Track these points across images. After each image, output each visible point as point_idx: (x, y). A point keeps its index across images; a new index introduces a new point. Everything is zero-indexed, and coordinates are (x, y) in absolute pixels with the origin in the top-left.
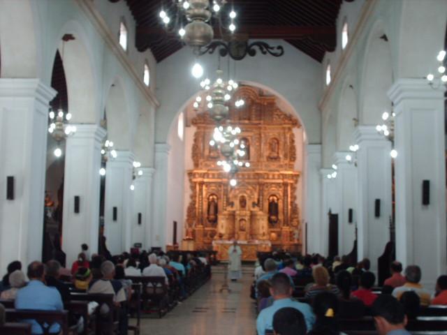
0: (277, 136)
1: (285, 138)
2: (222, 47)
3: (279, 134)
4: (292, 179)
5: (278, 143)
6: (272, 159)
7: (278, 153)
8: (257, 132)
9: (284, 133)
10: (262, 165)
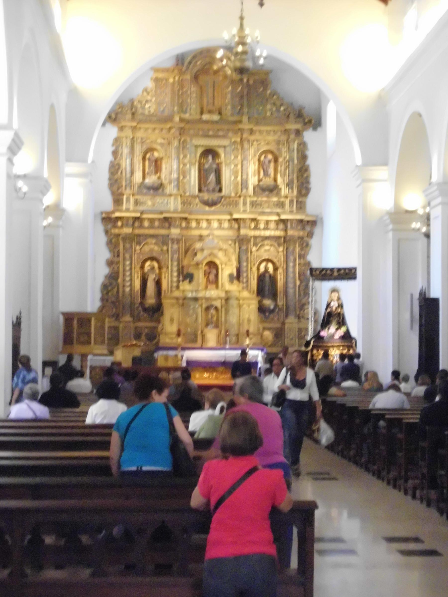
3: (278, 143)
4: (303, 229)
5: (276, 160)
7: (275, 180)
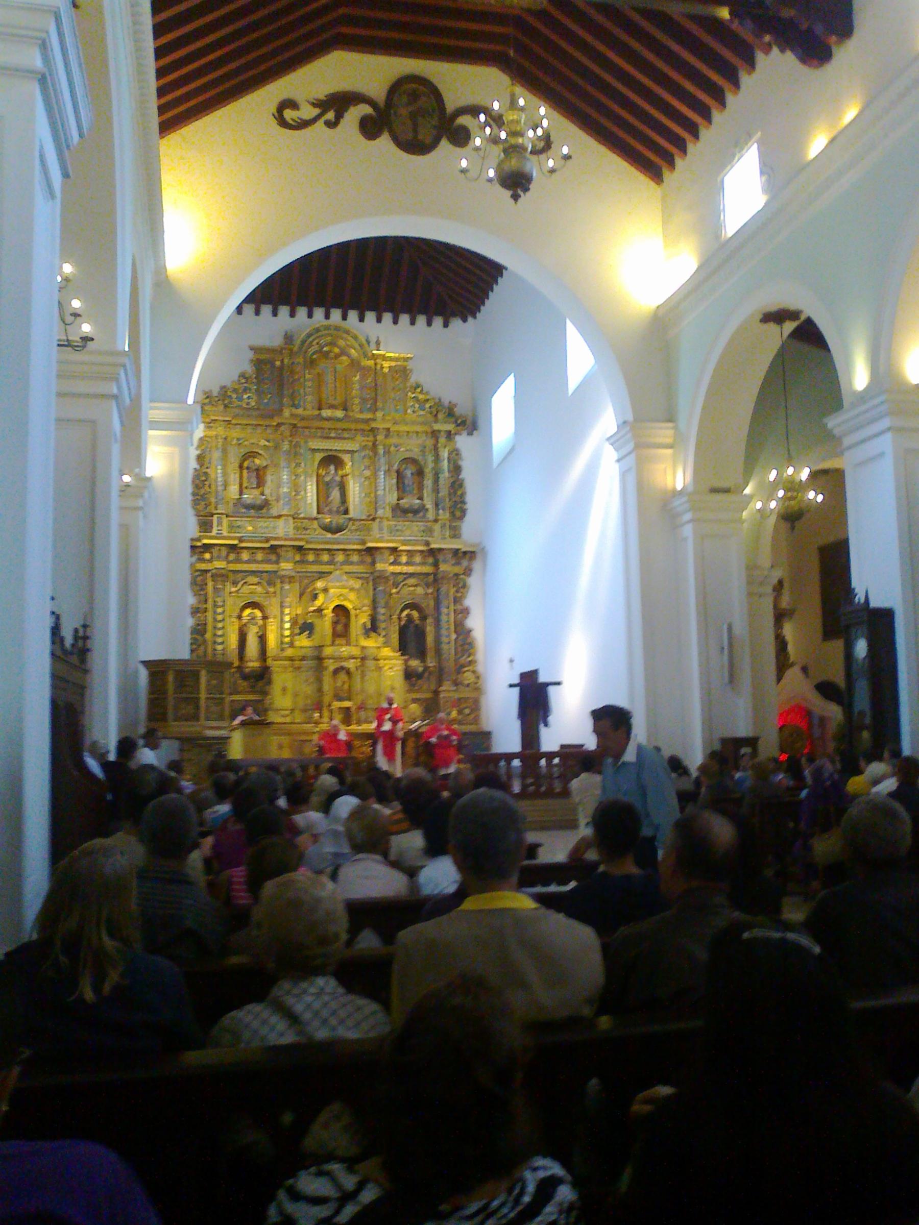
0: (415, 453)
1: (437, 458)
2: (366, 109)
5: (420, 473)
6: (405, 511)
7: (421, 498)
8: (368, 440)
9: (436, 448)
10: (381, 529)
